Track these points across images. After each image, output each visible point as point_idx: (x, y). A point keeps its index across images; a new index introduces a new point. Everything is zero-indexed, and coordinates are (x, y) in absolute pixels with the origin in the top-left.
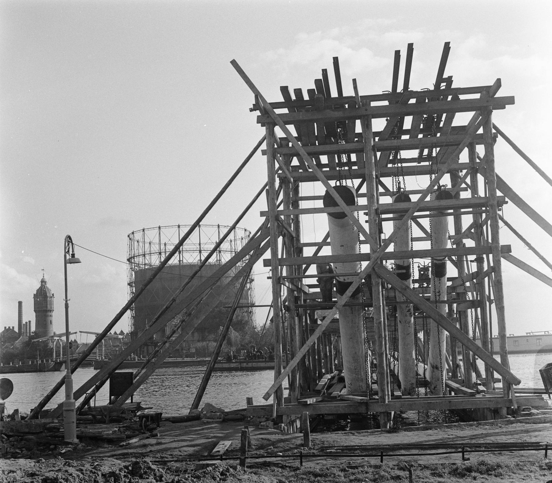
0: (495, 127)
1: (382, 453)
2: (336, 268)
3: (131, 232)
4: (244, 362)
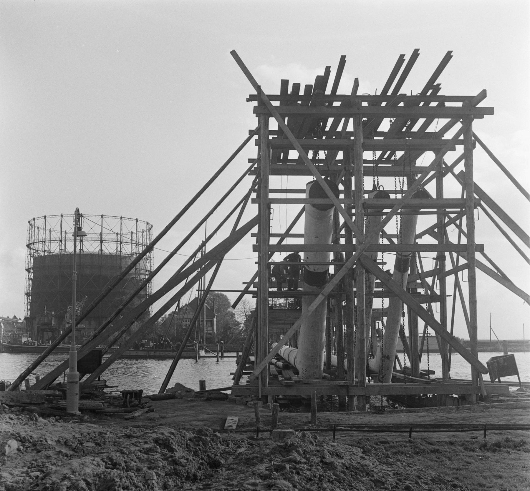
0: (475, 135)
1: (411, 429)
2: (308, 258)
3: (32, 218)
4: (152, 351)
